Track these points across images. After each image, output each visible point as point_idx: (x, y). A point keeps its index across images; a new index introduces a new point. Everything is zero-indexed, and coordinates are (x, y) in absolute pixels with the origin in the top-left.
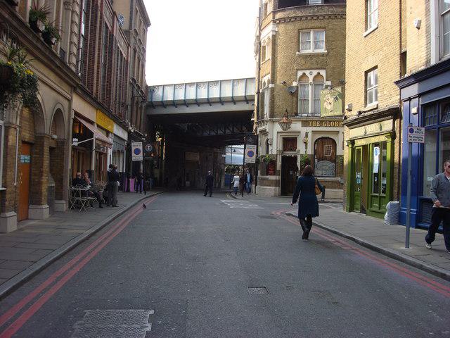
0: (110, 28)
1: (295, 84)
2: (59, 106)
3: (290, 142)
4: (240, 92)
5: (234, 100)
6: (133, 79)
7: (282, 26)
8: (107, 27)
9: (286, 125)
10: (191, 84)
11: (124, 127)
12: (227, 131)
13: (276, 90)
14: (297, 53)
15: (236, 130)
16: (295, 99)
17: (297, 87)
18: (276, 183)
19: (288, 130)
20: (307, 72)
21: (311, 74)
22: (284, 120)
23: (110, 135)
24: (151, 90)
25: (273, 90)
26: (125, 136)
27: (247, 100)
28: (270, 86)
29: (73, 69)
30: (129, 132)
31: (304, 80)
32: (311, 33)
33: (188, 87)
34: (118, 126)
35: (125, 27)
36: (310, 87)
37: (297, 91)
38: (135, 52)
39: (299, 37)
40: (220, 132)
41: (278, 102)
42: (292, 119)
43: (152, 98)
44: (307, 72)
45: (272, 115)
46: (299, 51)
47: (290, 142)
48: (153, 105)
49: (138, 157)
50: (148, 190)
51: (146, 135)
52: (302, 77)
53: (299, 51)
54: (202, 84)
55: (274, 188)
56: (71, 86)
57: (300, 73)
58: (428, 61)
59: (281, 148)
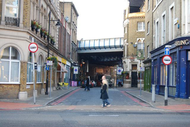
0: (69, 33)
1: (136, 43)
2: (41, 54)
3: (134, 66)
4: (118, 43)
5: (115, 47)
6: (73, 42)
7: (131, 20)
8: (64, 27)
9: (132, 59)
10: (97, 40)
11: (70, 62)
12: (115, 59)
13: (129, 46)
14: (137, 31)
15: (119, 59)
16: (136, 49)
17: (137, 45)
18: (129, 82)
19: (133, 62)
20: (141, 39)
21: (142, 39)
22: (132, 57)
23: (65, 65)
24: (79, 42)
25: (128, 46)
26: (69, 64)
27: (121, 47)
28: (127, 44)
29: (57, 48)
30: (71, 63)
31: (139, 41)
32: (142, 23)
33: (95, 41)
34: (68, 62)
35: (69, 21)
36: (142, 44)
37: (137, 46)
38: (74, 32)
39: (137, 24)
40: (111, 59)
41: (130, 51)
42: (135, 57)
43: (80, 46)
44: (141, 39)
45: (127, 56)
46: (137, 30)
47: (134, 66)
48: (80, 49)
49: (76, 73)
50: (79, 86)
51: (77, 62)
52: (138, 40)
53: (137, 30)
54: (102, 40)
55: (128, 84)
56: (56, 53)
57: (138, 39)
58: (157, 47)
59: (131, 68)
